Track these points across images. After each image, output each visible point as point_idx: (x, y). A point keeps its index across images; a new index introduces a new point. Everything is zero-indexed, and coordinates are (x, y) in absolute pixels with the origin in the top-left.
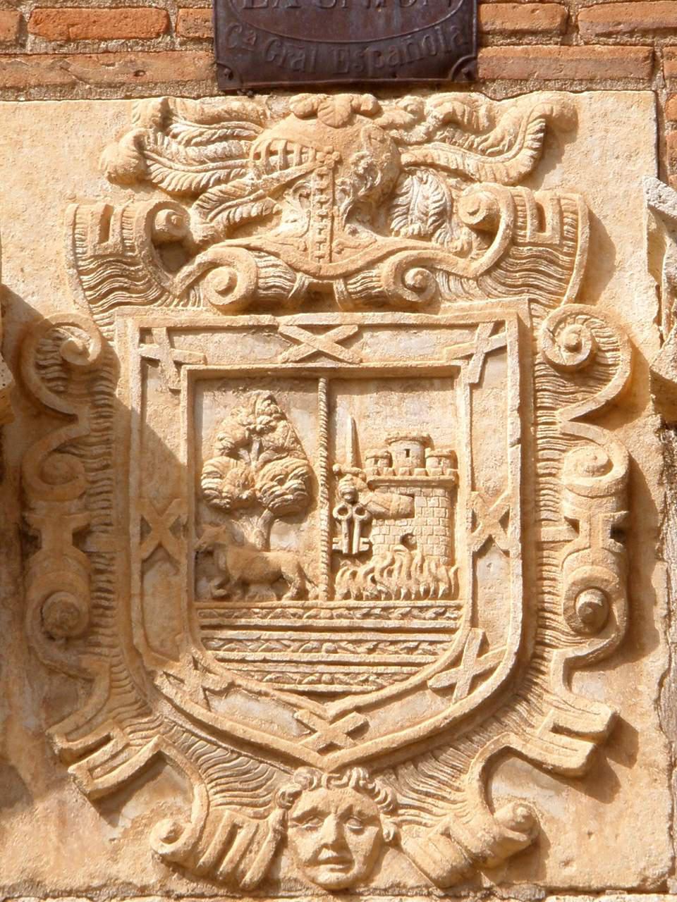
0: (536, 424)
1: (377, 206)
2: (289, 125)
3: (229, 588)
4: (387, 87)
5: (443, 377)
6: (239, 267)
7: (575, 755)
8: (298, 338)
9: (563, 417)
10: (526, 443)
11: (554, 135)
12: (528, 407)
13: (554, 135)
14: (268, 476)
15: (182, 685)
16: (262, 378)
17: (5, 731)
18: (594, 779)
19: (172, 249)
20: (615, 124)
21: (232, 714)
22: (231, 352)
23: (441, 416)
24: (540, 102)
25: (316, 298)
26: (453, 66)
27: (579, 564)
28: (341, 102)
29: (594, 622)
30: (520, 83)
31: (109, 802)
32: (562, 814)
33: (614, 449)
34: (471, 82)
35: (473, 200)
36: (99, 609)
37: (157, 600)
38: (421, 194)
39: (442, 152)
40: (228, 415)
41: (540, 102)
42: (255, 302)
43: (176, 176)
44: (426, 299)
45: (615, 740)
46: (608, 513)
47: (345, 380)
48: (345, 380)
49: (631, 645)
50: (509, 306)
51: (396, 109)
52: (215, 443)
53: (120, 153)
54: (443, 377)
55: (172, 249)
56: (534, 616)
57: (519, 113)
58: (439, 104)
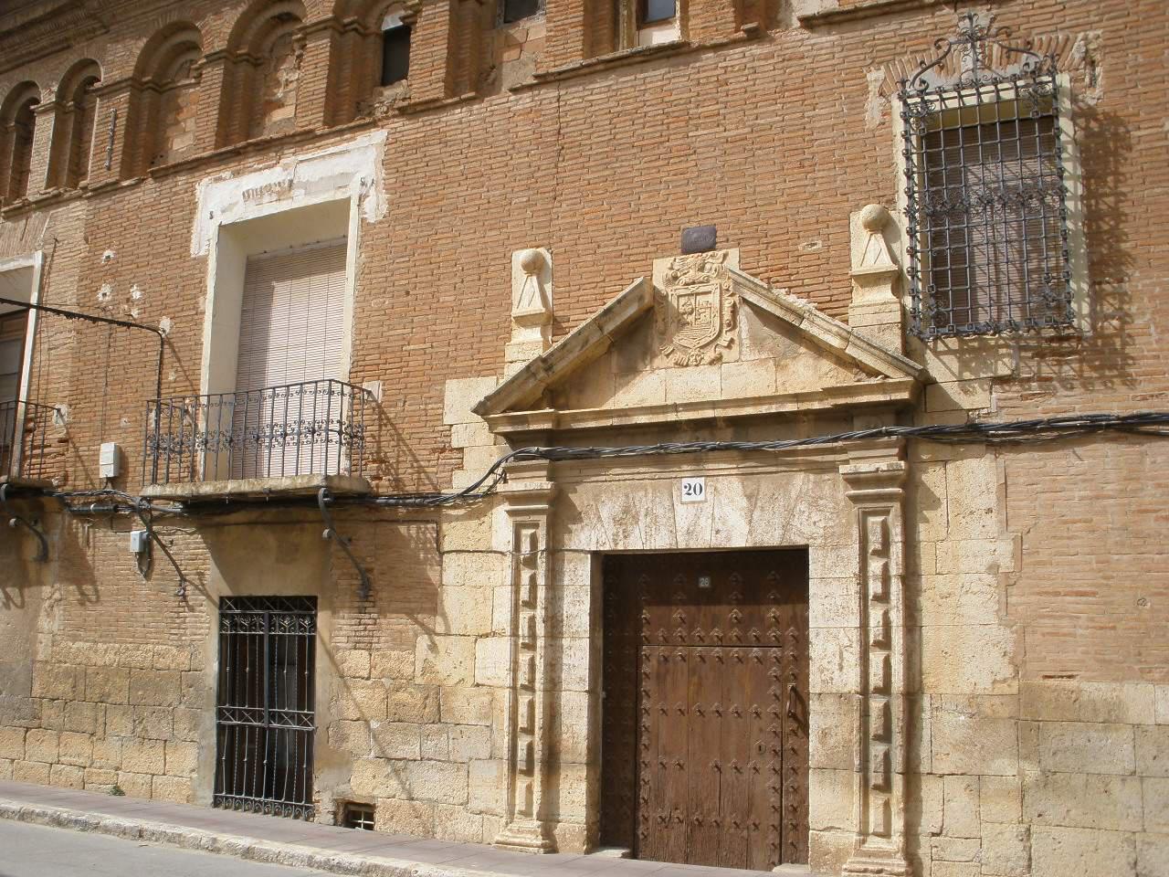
0: (1081, 361)
1: (702, 269)
2: (691, 258)
3: (682, 324)
4: (703, 252)
5: (710, 292)
6: (684, 279)
7: (726, 344)
8: (692, 289)
9: (726, 296)
10: (721, 301)
11: (725, 256)
12: (721, 293)
13: (725, 256)
14: (688, 309)
15: (676, 340)
16: (913, 641)
17: (347, 870)
18: (729, 347)
19: (675, 278)
20: (734, 253)
21: (682, 342)
22: (683, 292)
23: (710, 298)
24: (724, 251)
25: (694, 283)
26: (712, 248)
27: (727, 316)
28: (696, 255)
29: (729, 325)
30: (721, 249)
31: (668, 356)
32: (725, 352)
33: (731, 300)
34: (715, 250)
35: (714, 266)
36: (666, 330)
37: (673, 327)
38: (708, 266)
39: (710, 260)
40: (682, 301)
41: (724, 251)
42: (686, 284)
43: (676, 268)
44: (708, 281)
45: (732, 341)
46: (730, 309)
47: (697, 294)
48: (697, 294)
49: (734, 327)
50: (718, 281)
51: (704, 255)
52: (681, 305)
53: (669, 266)
54: (710, 292)
55: (675, 278)
56: (721, 325)
57: (720, 253)
58: (711, 253)
